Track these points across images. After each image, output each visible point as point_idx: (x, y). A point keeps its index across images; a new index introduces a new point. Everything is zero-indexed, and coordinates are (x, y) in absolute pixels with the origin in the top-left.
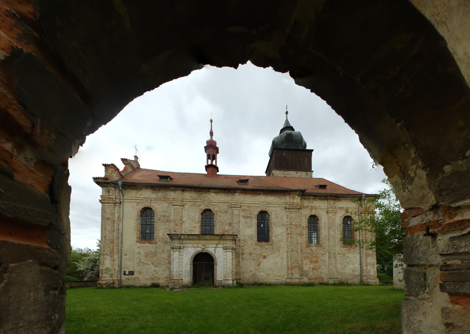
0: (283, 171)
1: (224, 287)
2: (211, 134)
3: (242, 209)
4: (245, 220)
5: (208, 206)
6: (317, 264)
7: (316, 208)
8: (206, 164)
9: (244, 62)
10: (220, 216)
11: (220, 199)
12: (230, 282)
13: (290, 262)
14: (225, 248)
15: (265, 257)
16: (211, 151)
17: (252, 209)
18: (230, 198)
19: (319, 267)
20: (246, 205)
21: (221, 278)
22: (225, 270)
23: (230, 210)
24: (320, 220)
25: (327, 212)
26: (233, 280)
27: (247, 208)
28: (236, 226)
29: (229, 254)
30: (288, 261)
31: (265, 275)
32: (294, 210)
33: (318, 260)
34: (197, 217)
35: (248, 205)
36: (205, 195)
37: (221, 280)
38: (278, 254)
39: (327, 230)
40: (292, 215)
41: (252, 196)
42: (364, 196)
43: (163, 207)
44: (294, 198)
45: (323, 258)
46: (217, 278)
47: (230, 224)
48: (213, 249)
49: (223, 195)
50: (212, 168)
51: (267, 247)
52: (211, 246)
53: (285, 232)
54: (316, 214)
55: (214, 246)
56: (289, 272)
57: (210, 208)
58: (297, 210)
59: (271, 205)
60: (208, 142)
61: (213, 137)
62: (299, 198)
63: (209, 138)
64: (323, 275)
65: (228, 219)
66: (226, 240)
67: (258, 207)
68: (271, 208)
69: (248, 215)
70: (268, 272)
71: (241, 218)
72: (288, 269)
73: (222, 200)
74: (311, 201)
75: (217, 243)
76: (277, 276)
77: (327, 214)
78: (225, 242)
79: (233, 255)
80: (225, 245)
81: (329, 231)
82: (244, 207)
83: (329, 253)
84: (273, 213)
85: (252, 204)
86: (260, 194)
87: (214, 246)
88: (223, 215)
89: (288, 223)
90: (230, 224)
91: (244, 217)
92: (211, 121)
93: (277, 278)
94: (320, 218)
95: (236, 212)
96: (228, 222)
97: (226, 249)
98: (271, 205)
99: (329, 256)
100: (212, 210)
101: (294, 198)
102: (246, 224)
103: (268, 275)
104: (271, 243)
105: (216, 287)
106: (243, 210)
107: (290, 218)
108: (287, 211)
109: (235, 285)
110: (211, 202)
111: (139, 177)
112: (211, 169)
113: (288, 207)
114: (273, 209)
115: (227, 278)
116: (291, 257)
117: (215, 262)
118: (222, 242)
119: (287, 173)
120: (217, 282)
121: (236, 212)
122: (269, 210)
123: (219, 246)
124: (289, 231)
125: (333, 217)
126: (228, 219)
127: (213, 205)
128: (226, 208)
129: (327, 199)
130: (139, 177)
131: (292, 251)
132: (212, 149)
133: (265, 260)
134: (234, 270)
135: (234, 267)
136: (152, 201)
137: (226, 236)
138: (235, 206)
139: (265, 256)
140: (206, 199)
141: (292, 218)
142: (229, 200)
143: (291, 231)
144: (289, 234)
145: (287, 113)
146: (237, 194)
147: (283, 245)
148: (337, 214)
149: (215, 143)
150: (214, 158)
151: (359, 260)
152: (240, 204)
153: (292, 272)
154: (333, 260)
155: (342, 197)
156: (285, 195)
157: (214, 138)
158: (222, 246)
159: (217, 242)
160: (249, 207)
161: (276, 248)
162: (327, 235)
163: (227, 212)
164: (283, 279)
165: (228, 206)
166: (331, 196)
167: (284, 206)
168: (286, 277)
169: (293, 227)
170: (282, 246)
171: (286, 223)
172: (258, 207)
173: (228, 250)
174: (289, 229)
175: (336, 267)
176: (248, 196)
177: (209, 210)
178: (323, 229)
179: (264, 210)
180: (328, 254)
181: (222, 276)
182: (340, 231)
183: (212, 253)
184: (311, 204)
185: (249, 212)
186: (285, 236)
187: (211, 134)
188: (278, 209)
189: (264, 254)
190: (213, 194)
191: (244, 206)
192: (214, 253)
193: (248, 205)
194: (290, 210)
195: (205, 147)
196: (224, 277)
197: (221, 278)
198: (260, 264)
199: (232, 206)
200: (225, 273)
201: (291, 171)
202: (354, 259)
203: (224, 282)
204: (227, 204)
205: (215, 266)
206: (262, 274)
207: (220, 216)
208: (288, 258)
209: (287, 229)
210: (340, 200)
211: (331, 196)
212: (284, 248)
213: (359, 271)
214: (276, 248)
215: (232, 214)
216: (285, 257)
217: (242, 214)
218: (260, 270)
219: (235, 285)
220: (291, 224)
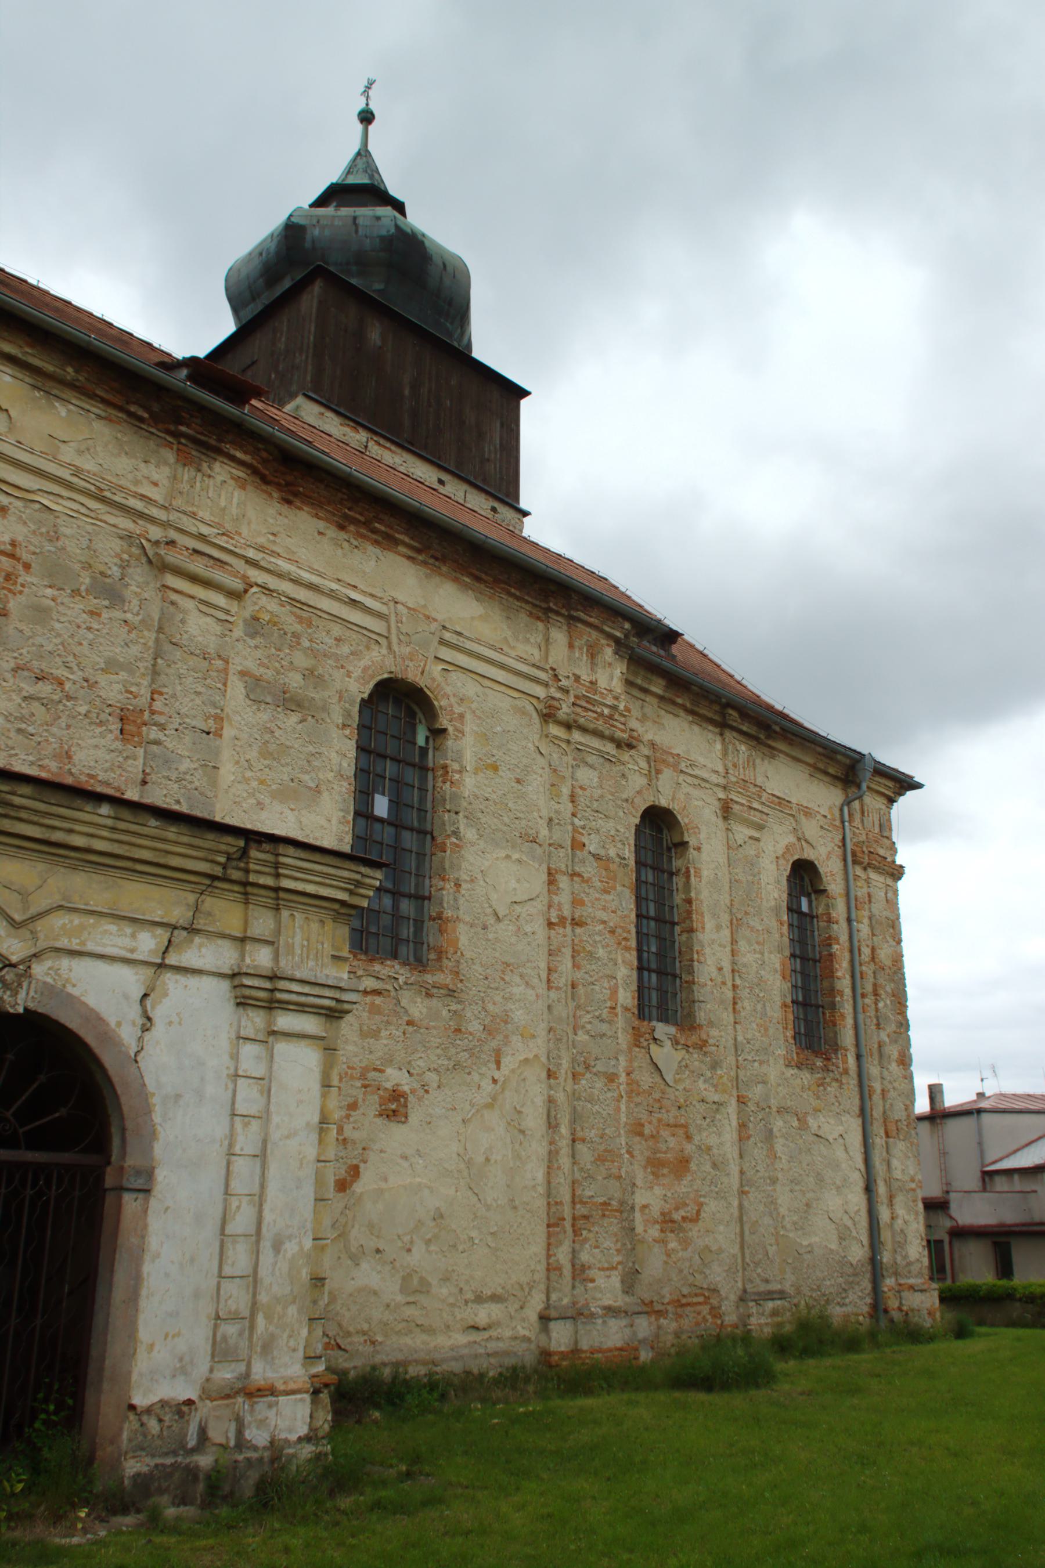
1: (215, 1490)
4: (264, 716)
6: (683, 1187)
10: (40, 614)
11: (68, 454)
13: (565, 1161)
14: (260, 995)
15: (395, 1107)
17: (325, 637)
19: (690, 1210)
20: (286, 587)
21: (182, 1369)
23: (139, 583)
24: (692, 853)
28: (181, 748)
30: (552, 1155)
31: (391, 1289)
32: (595, 743)
33: (689, 1148)
35: (302, 594)
37: (182, 1391)
38: (487, 1086)
39: (726, 933)
40: (586, 776)
41: (332, 532)
42: (869, 766)
45: (713, 1140)
46: (142, 1364)
47: (129, 724)
48: (132, 981)
51: (417, 1007)
52: (112, 938)
53: (540, 905)
54: (675, 807)
55: (147, 944)
56: (563, 1255)
58: (610, 748)
59: (462, 660)
62: (619, 669)
64: (717, 1275)
65: (111, 666)
66: (279, 897)
67: (373, 639)
68: (455, 676)
69: (295, 681)
70: (418, 1257)
71: (237, 688)
72: (553, 1224)
73: (88, 465)
75: (179, 914)
76: (479, 1299)
77: (720, 822)
78: (262, 923)
80: (262, 958)
81: (734, 942)
82: (264, 600)
83: (741, 1101)
84: (470, 726)
85: (332, 595)
86: (388, 542)
87: (147, 944)
88: (75, 610)
89: (557, 836)
91: (256, 688)
93: (483, 1314)
94: (692, 841)
95: (198, 627)
96: (111, 689)
97: (272, 1005)
98: (462, 660)
99: (742, 1126)
102: (265, 753)
103: (415, 1286)
104: (443, 978)
106: (255, 625)
107: (573, 798)
108: (554, 740)
113: (565, 710)
114: (470, 688)
115: (261, 1372)
116: (576, 1117)
118: (225, 911)
121: (198, 627)
122: (453, 691)
123: (203, 954)
124: (564, 898)
126: (111, 666)
131: (582, 1067)
133: (396, 1138)
137: (290, 858)
138: (198, 566)
139: (396, 1095)
141: (582, 801)
143: (577, 902)
144: (562, 920)
145: (367, 118)
146: (221, 471)
147: (525, 1003)
153: (585, 1257)
154: (757, 1152)
156: (544, 614)
159: (170, 903)
161: (475, 1027)
162: (727, 967)
164: (511, 1332)
165: (128, 537)
167: (540, 691)
168: (536, 1303)
169: (589, 869)
170: (519, 1016)
171: (544, 832)
172: (373, 639)
173: (285, 1021)
174: (564, 882)
175: (772, 1203)
178: (709, 924)
179: (412, 675)
180: (732, 1108)
181: (196, 1338)
182: (780, 950)
183: (109, 1037)
185: (301, 660)
186: (538, 926)
188: (501, 701)
189: (394, 1077)
191: (266, 590)
192: (128, 1035)
193: (302, 594)
194: (577, 736)
196: (220, 1352)
198: (355, 1172)
199: (172, 557)
204: (125, 523)
205: (130, 1203)
206: (369, 1274)
207: (40, 614)
208: (552, 1125)
209: (552, 880)
212: (528, 1036)
214: (475, 1027)
215: (165, 637)
216: (534, 1120)
217: (247, 656)
218: (357, 1235)
220: (577, 845)
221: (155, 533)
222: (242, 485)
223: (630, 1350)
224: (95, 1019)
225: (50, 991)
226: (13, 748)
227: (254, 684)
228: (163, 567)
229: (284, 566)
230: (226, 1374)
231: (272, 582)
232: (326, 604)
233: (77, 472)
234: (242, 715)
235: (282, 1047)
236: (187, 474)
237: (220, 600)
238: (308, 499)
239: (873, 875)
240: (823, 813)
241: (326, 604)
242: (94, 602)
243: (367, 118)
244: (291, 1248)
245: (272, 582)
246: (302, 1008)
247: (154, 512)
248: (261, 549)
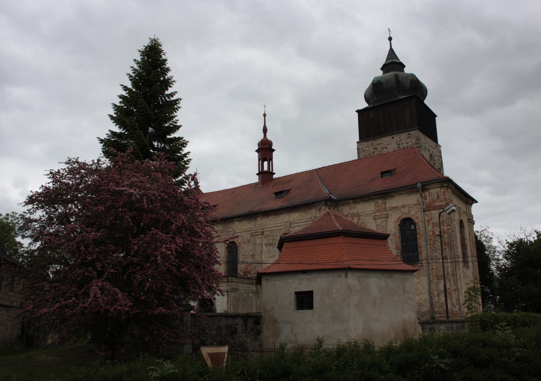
0: (371, 142)
2: (265, 130)
7: (358, 215)
9: (111, 145)
10: (243, 248)
11: (244, 228)
17: (275, 234)
18: (253, 224)
23: (252, 239)
25: (375, 219)
27: (270, 234)
34: (223, 252)
35: (271, 229)
36: (230, 225)
41: (274, 217)
44: (320, 210)
49: (246, 222)
50: (266, 176)
61: (267, 134)
69: (271, 242)
71: (264, 246)
73: (246, 227)
74: (352, 206)
77: (374, 221)
85: (274, 227)
86: (282, 213)
90: (253, 256)
92: (265, 115)
96: (251, 253)
101: (320, 210)
106: (266, 237)
119: (378, 142)
121: (258, 241)
125: (384, 224)
126: (251, 250)
129: (373, 199)
132: (265, 150)
138: (256, 234)
140: (231, 230)
142: (252, 227)
145: (390, 39)
146: (259, 219)
148: (389, 218)
149: (270, 144)
150: (269, 159)
151: (427, 287)
152: (261, 230)
155: (396, 192)
156: (310, 208)
157: (269, 137)
160: (272, 232)
163: (249, 242)
166: (374, 195)
172: (281, 230)
176: (271, 218)
184: (353, 211)
185: (272, 238)
187: (265, 130)
190: (237, 223)
193: (271, 229)
195: (404, 66)
201: (383, 138)
202: (419, 286)
210: (392, 197)
211: (374, 195)
213: (428, 306)
215: (255, 243)
226: (417, 147)
227: (266, 244)
231: (266, 230)
232: (274, 228)
234: (265, 248)
237: (260, 236)
239: (432, 212)
240: (270, 287)
241: (274, 228)
243: (390, 39)
245: (266, 230)
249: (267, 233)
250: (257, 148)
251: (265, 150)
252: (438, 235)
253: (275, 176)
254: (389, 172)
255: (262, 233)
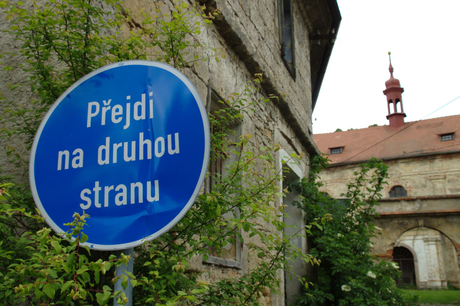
2: (391, 70)
3: (447, 179)
5: (397, 181)
8: (387, 114)
11: (414, 171)
12: (439, 284)
14: (426, 240)
16: (393, 95)
22: (430, 268)
23: (429, 184)
26: (442, 281)
29: (433, 248)
35: (456, 173)
37: (426, 280)
43: (340, 189)
50: (397, 118)
55: (412, 238)
57: (400, 184)
60: (387, 84)
61: (394, 73)
63: (387, 77)
73: (417, 170)
79: (437, 249)
80: (426, 236)
87: (412, 238)
92: (389, 54)
97: (428, 241)
100: (404, 185)
105: (419, 289)
106: (449, 181)
109: (446, 288)
110: (400, 176)
111: (293, 74)
112: (394, 118)
115: (434, 279)
117: (415, 259)
120: (420, 284)
123: (418, 237)
127: (404, 180)
128: (423, 181)
130: (293, 74)
132: (394, 91)
134: (442, 268)
135: (441, 264)
136: (328, 185)
138: (436, 178)
142: (427, 170)
149: (397, 82)
152: (443, 174)
157: (396, 76)
158: (422, 237)
165: (425, 178)
173: (430, 243)
177: (400, 187)
181: (426, 275)
183: (410, 247)
187: (391, 70)
192: (412, 247)
193: (456, 173)
196: (430, 277)
197: (425, 278)
200: (430, 272)
203: (430, 285)
204: (424, 176)
205: (415, 263)
219: (446, 288)
221: (429, 175)
222: (441, 161)
223: (345, 258)
224: (408, 246)
225: (403, 244)
228: (431, 180)
229: (451, 170)
230: (430, 279)
231: (450, 173)
233: (415, 172)
235: (430, 246)
236: (432, 164)
237: (441, 180)
238: (453, 157)
242: (422, 188)
244: (436, 267)
245: (450, 173)
246: (432, 241)
247: (428, 172)
248: (447, 169)
249: (451, 177)
250: (385, 88)
251: (394, 91)
252: (363, 301)
253: (406, 120)
254: (339, 148)
255: (445, 177)
